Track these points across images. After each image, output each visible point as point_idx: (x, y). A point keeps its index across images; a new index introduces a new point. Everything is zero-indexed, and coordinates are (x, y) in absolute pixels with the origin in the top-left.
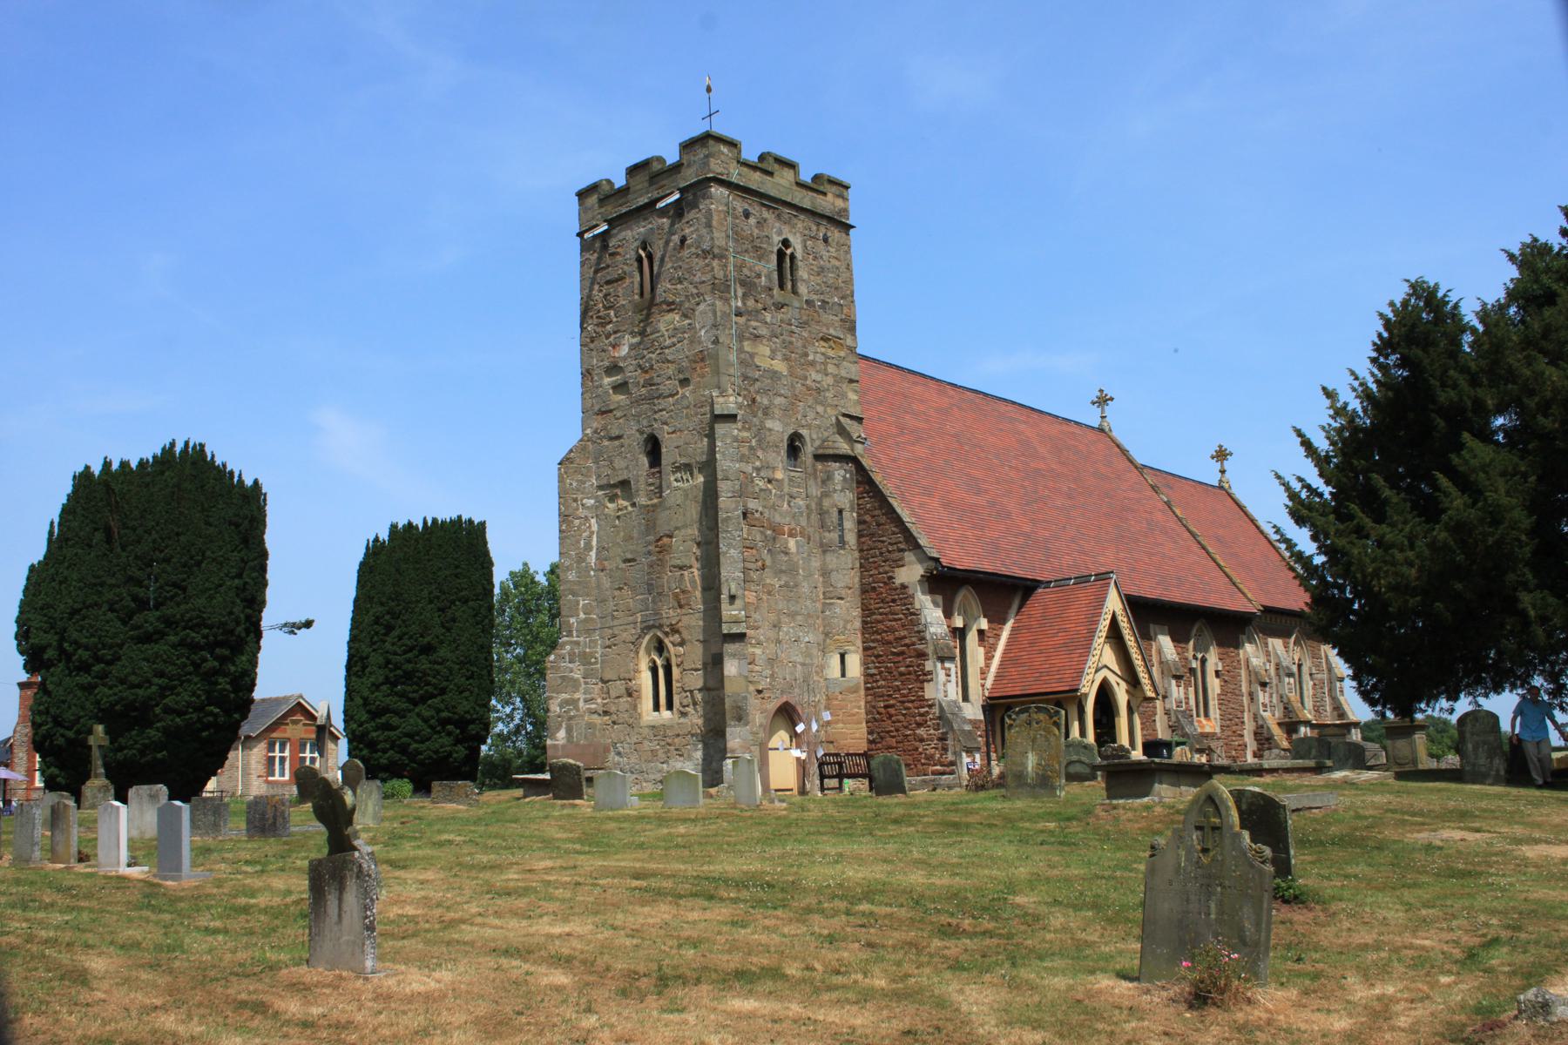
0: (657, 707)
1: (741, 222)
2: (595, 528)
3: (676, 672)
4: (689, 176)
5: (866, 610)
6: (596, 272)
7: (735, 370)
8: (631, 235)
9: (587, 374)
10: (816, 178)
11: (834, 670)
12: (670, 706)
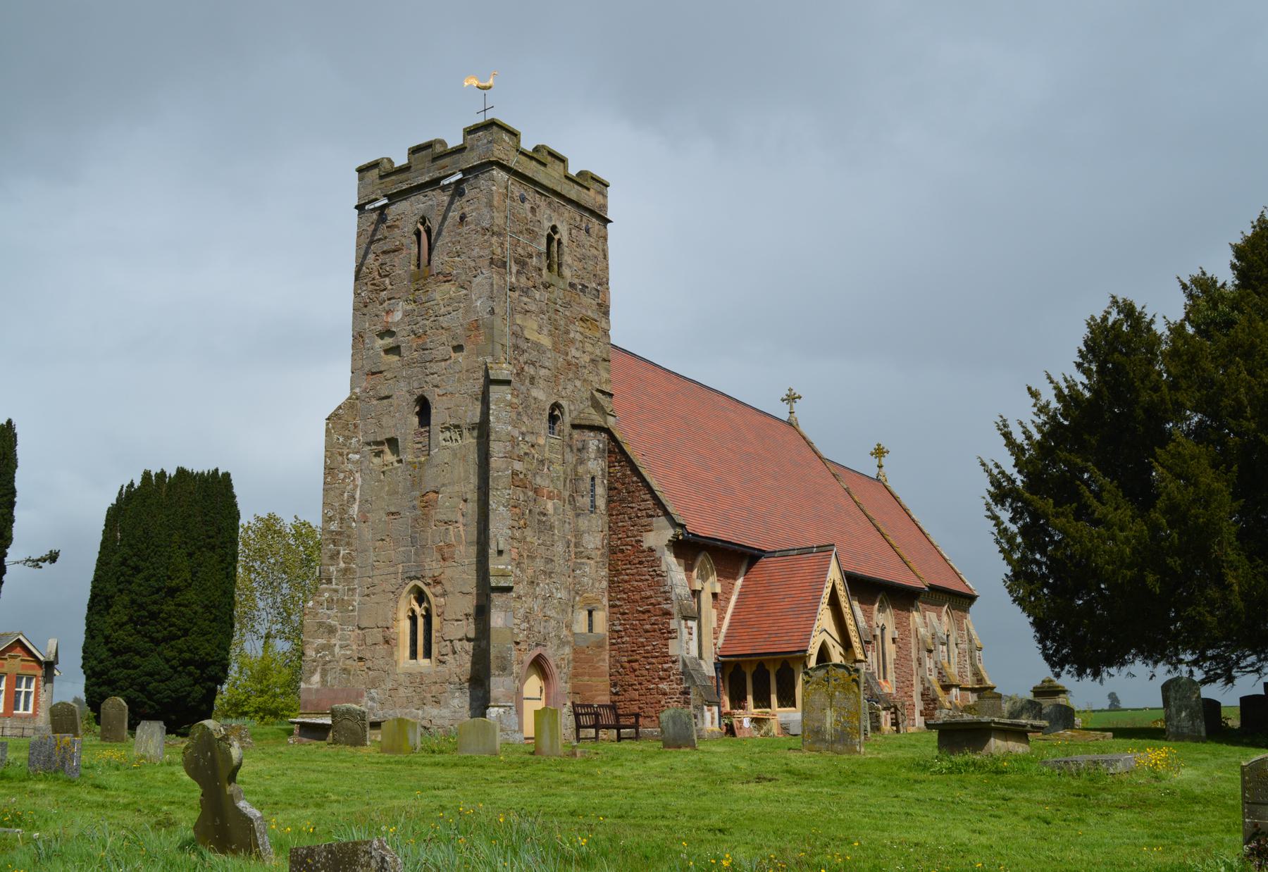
0: (414, 655)
1: (517, 204)
2: (359, 482)
3: (436, 621)
4: (472, 159)
5: (614, 571)
6: (372, 242)
7: (508, 341)
8: (408, 210)
9: (358, 337)
10: (581, 174)
11: (581, 625)
12: (428, 654)
